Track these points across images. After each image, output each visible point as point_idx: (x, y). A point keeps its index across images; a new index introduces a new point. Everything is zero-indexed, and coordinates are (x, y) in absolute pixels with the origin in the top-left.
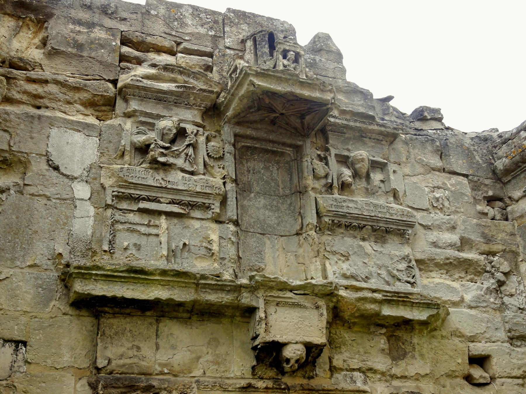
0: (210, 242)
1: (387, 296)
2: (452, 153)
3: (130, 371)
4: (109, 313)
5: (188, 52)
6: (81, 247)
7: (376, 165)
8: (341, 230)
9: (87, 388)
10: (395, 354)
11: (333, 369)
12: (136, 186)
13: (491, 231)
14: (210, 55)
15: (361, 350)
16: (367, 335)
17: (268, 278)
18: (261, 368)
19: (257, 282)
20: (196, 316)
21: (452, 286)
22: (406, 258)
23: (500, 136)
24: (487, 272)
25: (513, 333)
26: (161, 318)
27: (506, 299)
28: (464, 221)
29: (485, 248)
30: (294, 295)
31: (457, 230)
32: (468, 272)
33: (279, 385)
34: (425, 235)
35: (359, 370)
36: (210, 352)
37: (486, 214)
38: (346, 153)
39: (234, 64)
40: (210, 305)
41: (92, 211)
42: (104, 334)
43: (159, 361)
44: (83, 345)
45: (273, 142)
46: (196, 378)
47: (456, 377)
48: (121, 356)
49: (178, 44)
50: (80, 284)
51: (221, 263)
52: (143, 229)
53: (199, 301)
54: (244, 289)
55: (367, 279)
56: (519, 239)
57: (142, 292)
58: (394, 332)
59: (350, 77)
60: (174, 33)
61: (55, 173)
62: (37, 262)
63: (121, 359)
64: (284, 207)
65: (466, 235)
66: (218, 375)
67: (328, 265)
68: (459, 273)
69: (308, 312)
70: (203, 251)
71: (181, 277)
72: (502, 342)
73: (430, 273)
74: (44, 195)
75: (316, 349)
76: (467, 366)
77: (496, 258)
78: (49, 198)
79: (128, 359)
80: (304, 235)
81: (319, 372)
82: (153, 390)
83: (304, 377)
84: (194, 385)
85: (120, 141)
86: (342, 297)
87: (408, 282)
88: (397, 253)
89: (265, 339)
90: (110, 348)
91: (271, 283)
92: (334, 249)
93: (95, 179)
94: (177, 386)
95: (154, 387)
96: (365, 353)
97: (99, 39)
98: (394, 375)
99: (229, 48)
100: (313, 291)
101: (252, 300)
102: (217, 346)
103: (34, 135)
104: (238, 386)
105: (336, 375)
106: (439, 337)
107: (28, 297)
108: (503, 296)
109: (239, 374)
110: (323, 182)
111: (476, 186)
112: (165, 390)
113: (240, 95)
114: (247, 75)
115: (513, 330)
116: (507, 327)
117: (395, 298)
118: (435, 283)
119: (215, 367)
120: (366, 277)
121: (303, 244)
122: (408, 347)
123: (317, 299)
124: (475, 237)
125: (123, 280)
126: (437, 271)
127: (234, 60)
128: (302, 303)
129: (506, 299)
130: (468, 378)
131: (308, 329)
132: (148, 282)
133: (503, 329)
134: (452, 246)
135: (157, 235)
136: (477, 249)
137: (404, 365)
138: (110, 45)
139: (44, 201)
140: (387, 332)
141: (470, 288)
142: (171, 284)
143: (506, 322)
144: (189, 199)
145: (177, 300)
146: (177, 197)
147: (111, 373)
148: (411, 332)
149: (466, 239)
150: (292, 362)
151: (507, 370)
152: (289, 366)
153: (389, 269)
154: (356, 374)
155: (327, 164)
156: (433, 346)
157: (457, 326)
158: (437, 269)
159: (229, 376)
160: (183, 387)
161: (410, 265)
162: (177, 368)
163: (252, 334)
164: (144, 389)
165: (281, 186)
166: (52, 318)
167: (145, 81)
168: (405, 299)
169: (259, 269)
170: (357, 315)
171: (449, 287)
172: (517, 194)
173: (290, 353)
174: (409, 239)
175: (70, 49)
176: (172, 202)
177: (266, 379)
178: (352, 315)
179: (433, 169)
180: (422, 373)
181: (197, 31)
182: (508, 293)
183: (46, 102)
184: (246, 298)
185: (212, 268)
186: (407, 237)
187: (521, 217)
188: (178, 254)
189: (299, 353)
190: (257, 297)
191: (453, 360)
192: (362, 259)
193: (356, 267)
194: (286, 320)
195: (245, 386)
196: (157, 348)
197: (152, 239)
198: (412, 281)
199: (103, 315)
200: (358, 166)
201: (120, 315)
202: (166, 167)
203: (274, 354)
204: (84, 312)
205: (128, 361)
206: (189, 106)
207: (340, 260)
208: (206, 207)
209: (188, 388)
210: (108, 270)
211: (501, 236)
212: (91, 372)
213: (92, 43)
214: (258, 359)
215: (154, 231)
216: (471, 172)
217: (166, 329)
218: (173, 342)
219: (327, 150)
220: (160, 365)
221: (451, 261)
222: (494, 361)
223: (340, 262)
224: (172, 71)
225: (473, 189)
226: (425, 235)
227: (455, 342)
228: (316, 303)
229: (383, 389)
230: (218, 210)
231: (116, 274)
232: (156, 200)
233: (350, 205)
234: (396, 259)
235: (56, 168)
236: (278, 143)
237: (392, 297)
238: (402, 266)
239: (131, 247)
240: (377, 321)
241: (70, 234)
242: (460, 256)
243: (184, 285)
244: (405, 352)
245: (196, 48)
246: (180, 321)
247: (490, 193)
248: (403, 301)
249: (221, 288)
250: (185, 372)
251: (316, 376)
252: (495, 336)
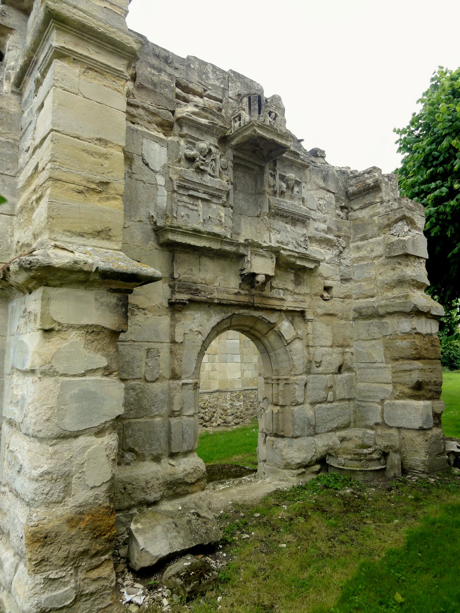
0: (221, 217)
2: (330, 179)
5: (210, 97)
6: (161, 213)
7: (298, 183)
8: (278, 217)
9: (168, 287)
11: (272, 288)
12: (188, 181)
14: (221, 101)
19: (249, 242)
22: (304, 235)
23: (352, 173)
27: (342, 260)
28: (330, 218)
29: (337, 233)
31: (327, 223)
35: (282, 289)
37: (340, 216)
38: (284, 174)
39: (239, 113)
41: (166, 193)
45: (250, 162)
48: (184, 273)
49: (205, 91)
52: (190, 206)
55: (287, 244)
56: (352, 231)
57: (198, 243)
59: (130, 27)
60: (203, 83)
61: (146, 168)
62: (142, 219)
64: (251, 200)
70: (218, 222)
74: (142, 181)
77: (341, 239)
78: (144, 183)
80: (261, 218)
85: (178, 152)
93: (166, 174)
97: (165, 81)
99: (231, 98)
103: (135, 142)
105: (273, 290)
107: (139, 238)
109: (234, 286)
110: (272, 189)
111: (338, 200)
113: (244, 134)
114: (253, 125)
124: (334, 228)
127: (239, 110)
129: (342, 260)
130: (322, 296)
132: (201, 237)
134: (323, 231)
135: (197, 210)
138: (171, 86)
139: (142, 184)
144: (212, 192)
146: (207, 190)
147: (180, 281)
150: (260, 283)
154: (281, 291)
155: (275, 179)
162: (208, 281)
163: (240, 268)
165: (250, 188)
167: (193, 116)
171: (320, 252)
172: (356, 207)
175: (150, 86)
176: (205, 193)
178: (283, 263)
179: (320, 188)
180: (307, 292)
181: (215, 83)
183: (137, 120)
187: (356, 219)
188: (206, 221)
197: (195, 212)
200: (290, 182)
202: (203, 172)
205: (187, 276)
206: (212, 135)
208: (219, 197)
211: (345, 228)
213: (161, 83)
215: (196, 208)
216: (336, 192)
219: (275, 170)
220: (201, 279)
222: (334, 290)
224: (206, 111)
225: (336, 201)
230: (225, 200)
232: (197, 190)
233: (285, 204)
235: (147, 165)
236: (253, 163)
238: (302, 239)
239: (185, 216)
241: (156, 206)
245: (214, 95)
247: (343, 205)
249: (231, 243)
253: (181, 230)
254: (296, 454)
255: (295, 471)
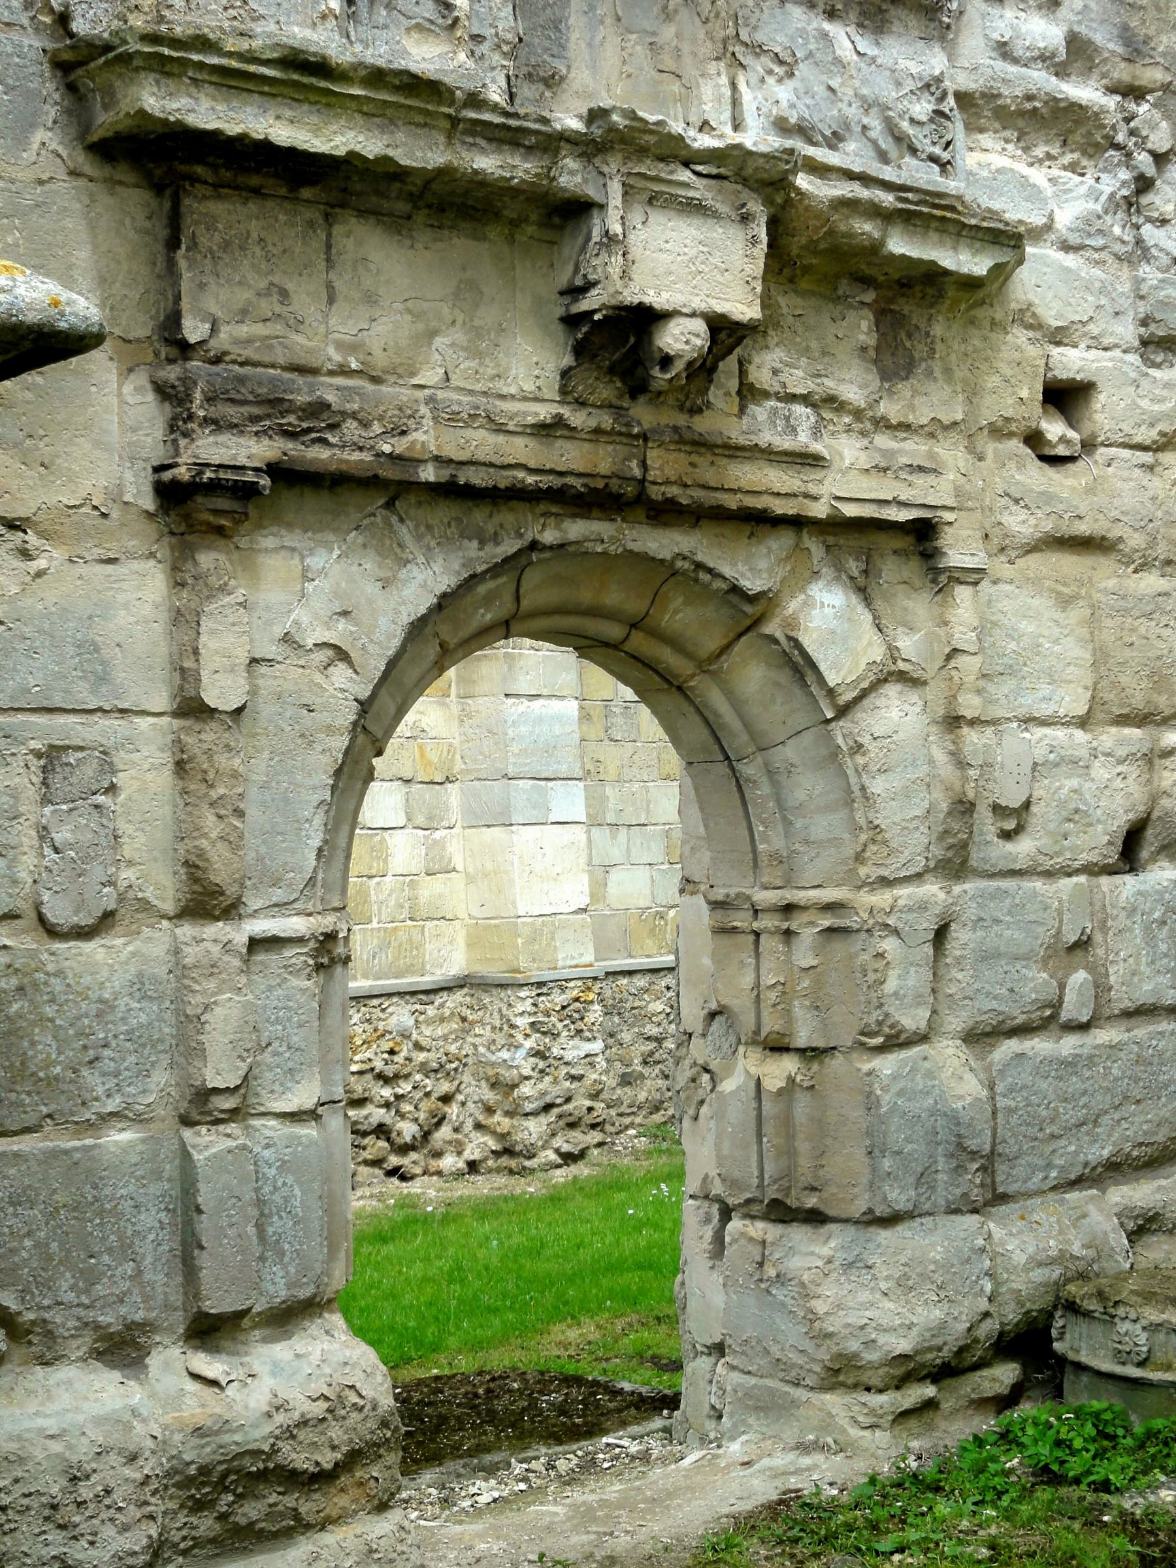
1: (906, 200)
3: (267, 359)
4: (206, 183)
10: (888, 361)
11: (748, 393)
13: (1144, 21)
15: (814, 344)
16: (831, 305)
17: (642, 120)
18: (587, 374)
19: (612, 129)
20: (426, 211)
21: (1031, 181)
22: (931, 86)
24: (1118, 147)
25: (1153, 327)
26: (337, 210)
27: (1148, 230)
29: (1122, 73)
30: (694, 177)
32: (1069, 142)
33: (628, 425)
34: (983, 16)
35: (805, 399)
36: (460, 321)
40: (479, 181)
42: (195, 244)
43: (336, 335)
44: (129, 272)
46: (427, 392)
47: (1011, 435)
48: (243, 315)
50: (155, 90)
51: (473, 52)
53: (456, 170)
54: (568, 146)
57: (316, 131)
58: (891, 301)
63: (243, 322)
65: (1082, 29)
66: (478, 387)
67: (742, 87)
68: (1047, 142)
69: (720, 231)
71: (417, 96)
72: (1125, 352)
73: (980, 136)
75: (729, 336)
76: (1038, 409)
77: (1144, 108)
79: (260, 325)
81: (716, 396)
82: (325, 415)
83: (681, 408)
84: (424, 410)
86: (798, 191)
87: (933, 159)
88: (915, 69)
89: (621, 298)
90: (213, 287)
91: (647, 137)
92: (760, 37)
94: (382, 408)
95: (329, 406)
96: (824, 354)
98: (882, 418)
100: (741, 169)
101: (585, 181)
102: (476, 306)
104: (530, 420)
105: (753, 408)
106: (987, 324)
108: (1141, 220)
112: (355, 418)
115: (1154, 321)
116: (1142, 310)
117: (925, 210)
118: (993, 167)
119: (473, 364)
120: (834, 133)
121: (676, 11)
122: (920, 347)
123: (746, 194)
124: (1103, 38)
125: (266, 89)
126: (996, 132)
128: (710, 203)
129: (1148, 230)
130: (1034, 439)
131: (719, 278)
132: (330, 103)
133: (1131, 313)
134: (1045, 58)
136: (1104, 76)
137: (908, 394)
140: (875, 301)
141: (1070, 190)
142: (389, 112)
143: (1142, 298)
145: (402, 162)
147: (217, 360)
148: (931, 306)
149: (1082, 40)
150: (679, 366)
151: (1124, 426)
152: (668, 376)
153: (891, 113)
154: (799, 410)
156: (970, 348)
157: (1031, 297)
158: (997, 125)
159: (505, 391)
160: (396, 412)
161: (941, 107)
162: (380, 360)
163: (564, 278)
164: (303, 410)
166: (41, 182)
168: (949, 215)
169: (553, 76)
170: (823, 245)
171: (1024, 183)
173: (677, 340)
174: (948, 27)
177: (594, 406)
178: (812, 248)
180: (946, 419)
182: (1156, 215)
184: (572, 173)
185: (452, 65)
186: (946, 20)
189: (699, 342)
190: (602, 174)
191: (1010, 390)
192: (824, 77)
193: (809, 101)
194: (668, 246)
195: (548, 421)
196: (331, 300)
198: (945, 156)
199: (188, 187)
201: (230, 192)
203: (632, 340)
204: (124, 173)
205: (260, 330)
207: (770, 72)
209: (410, 417)
210: (230, 55)
212: (157, 354)
214: (580, 350)
217: (350, 243)
218: (367, 282)
221: (1038, 104)
222: (1100, 400)
223: (771, 80)
226: (983, 16)
227: (1019, 341)
228: (744, 205)
229: (857, 453)
231: (252, 68)
234: (909, 85)
237: (917, 204)
238: (922, 108)
240: (863, 267)
242: (1061, 92)
243: (420, 119)
244: (912, 358)
246: (384, 223)
248: (943, 218)
250: (400, 370)
251: (708, 408)
252: (1111, 334)
253: (214, 60)
254: (888, 1310)
255: (883, 1398)
